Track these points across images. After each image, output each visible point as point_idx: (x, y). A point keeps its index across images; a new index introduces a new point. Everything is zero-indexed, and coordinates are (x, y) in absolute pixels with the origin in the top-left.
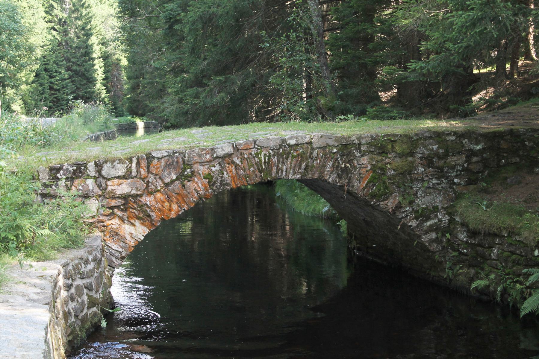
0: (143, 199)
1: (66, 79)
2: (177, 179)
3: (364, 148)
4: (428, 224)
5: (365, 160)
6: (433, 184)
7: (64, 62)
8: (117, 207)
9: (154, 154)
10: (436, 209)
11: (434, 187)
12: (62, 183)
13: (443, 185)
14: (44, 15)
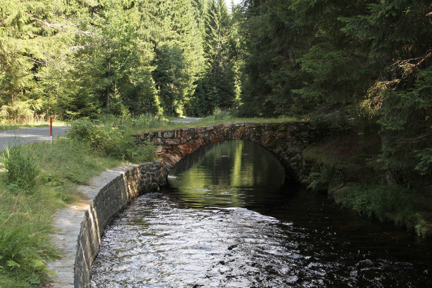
0: (179, 146)
1: (216, 94)
2: (192, 139)
3: (266, 128)
4: (293, 159)
5: (266, 133)
6: (295, 143)
7: (215, 83)
8: (169, 149)
9: (183, 130)
10: (296, 153)
11: (295, 144)
12: (149, 139)
13: (299, 143)
14: (203, 53)
